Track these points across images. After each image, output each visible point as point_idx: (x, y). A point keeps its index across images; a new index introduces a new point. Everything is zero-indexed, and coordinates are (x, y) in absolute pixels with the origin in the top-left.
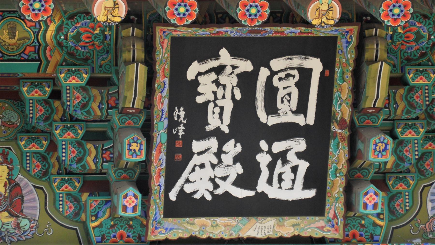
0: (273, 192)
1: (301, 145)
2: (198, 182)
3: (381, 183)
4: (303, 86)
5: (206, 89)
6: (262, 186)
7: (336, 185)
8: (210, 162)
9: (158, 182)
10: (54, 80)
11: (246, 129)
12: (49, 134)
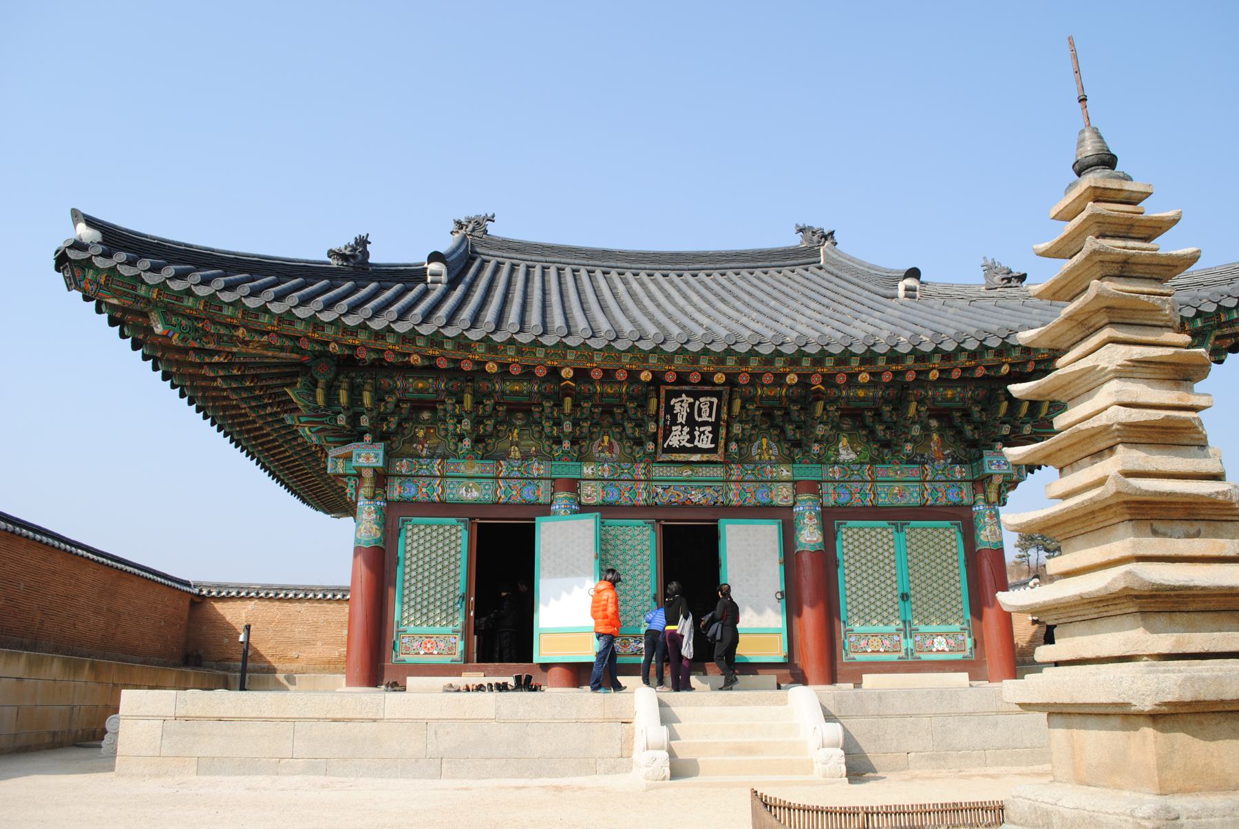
0: (700, 445)
1: (710, 428)
2: (674, 441)
3: (737, 441)
4: (711, 408)
5: (677, 409)
6: (696, 443)
7: (722, 443)
9: (660, 441)
10: (624, 406)
11: (691, 423)
12: (623, 425)
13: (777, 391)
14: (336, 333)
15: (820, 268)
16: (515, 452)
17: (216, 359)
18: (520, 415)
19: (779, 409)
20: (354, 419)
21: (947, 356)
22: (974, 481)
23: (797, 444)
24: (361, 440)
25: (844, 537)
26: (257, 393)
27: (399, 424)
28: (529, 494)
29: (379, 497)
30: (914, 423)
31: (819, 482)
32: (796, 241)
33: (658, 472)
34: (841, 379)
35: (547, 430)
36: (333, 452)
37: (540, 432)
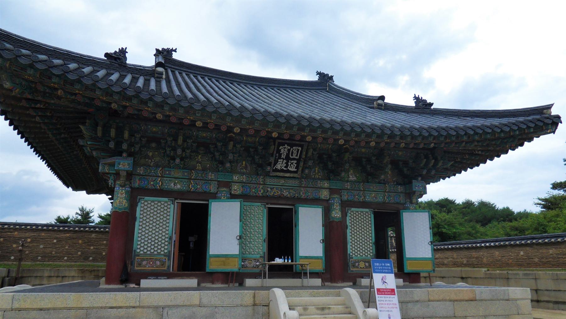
0: (290, 169)
1: (296, 162)
2: (278, 167)
4: (298, 152)
5: (282, 151)
6: (289, 168)
7: (300, 169)
8: (552, 105)
10: (166, 139)
11: (288, 158)
12: (165, 149)
14: (15, 93)
16: (199, 167)
17: (38, 106)
18: (202, 148)
20: (118, 144)
21: (358, 135)
22: (405, 193)
23: (260, 166)
24: (121, 155)
26: (59, 126)
29: (128, 186)
30: (310, 159)
31: (340, 189)
33: (269, 181)
35: (168, 152)
36: (102, 161)
37: (164, 153)
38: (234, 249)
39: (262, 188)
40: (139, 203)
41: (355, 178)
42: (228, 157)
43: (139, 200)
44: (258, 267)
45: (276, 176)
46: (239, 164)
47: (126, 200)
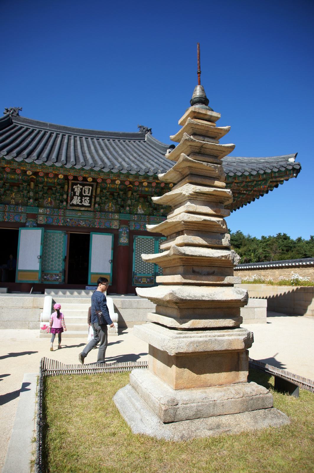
0: (84, 204)
6: (83, 203)
7: (93, 204)
9: (69, 201)
11: (81, 195)
13: (111, 186)
15: (145, 142)
18: (16, 188)
19: (116, 193)
25: (137, 241)
27: (5, 191)
28: (17, 219)
31: (129, 221)
32: (138, 131)
34: (137, 184)
38: (35, 266)
39: (63, 219)
40: (135, 240)
41: (143, 212)
42: (127, 202)
43: (135, 237)
44: (57, 280)
45: (73, 210)
46: (46, 200)
47: (127, 238)
